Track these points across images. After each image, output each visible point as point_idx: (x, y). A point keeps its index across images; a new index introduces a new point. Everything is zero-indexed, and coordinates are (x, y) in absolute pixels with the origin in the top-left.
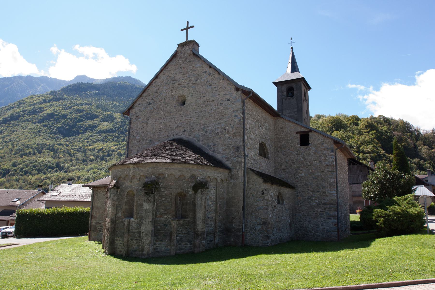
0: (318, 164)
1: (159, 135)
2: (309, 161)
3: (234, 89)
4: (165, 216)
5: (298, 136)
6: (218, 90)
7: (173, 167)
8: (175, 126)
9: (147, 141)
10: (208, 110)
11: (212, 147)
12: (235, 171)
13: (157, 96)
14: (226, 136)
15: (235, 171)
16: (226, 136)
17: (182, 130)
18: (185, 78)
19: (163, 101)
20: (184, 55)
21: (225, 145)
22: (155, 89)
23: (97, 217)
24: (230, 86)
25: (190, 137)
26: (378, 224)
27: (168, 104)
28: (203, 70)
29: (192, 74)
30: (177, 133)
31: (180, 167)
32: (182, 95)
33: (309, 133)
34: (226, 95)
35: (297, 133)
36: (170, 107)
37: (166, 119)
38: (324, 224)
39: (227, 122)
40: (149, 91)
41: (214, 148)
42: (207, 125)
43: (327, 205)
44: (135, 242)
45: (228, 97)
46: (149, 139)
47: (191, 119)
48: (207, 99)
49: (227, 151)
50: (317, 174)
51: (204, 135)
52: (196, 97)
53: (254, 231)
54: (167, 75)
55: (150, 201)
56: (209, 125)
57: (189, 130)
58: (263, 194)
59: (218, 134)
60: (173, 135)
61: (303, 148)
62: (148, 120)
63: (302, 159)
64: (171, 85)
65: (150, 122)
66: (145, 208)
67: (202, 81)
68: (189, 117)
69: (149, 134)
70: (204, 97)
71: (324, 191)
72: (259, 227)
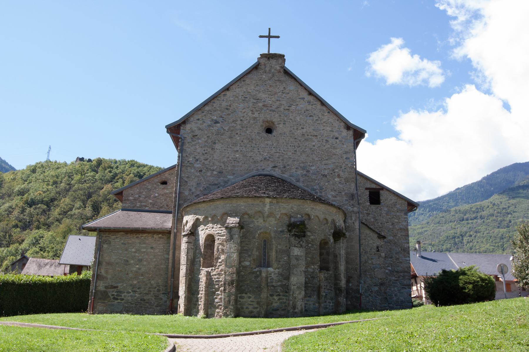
1: (233, 166)
3: (343, 127)
5: (367, 193)
6: (322, 124)
7: (317, 207)
8: (259, 158)
9: (215, 173)
10: (310, 146)
11: (317, 191)
12: (350, 221)
13: (229, 114)
14: (336, 180)
15: (350, 221)
16: (336, 180)
17: (272, 165)
18: (273, 99)
19: (239, 122)
20: (270, 71)
21: (335, 191)
22: (224, 104)
23: (109, 276)
24: (338, 122)
26: (467, 291)
27: (247, 127)
28: (299, 95)
29: (283, 96)
30: (263, 167)
31: (323, 208)
32: (269, 119)
34: (333, 132)
35: (367, 189)
36: (251, 132)
37: (246, 147)
38: (398, 294)
39: (337, 164)
40: (215, 105)
41: (321, 192)
42: (309, 164)
44: (276, 298)
45: (336, 135)
46: (218, 170)
47: (284, 152)
48: (306, 132)
49: (338, 198)
50: (389, 238)
51: (306, 175)
52: (291, 127)
53: (369, 293)
54: (245, 90)
55: (301, 246)
56: (311, 164)
57: (282, 166)
58: (378, 251)
60: (258, 170)
61: (373, 207)
62: (215, 143)
63: (372, 220)
64: (251, 105)
65: (218, 146)
66: (296, 254)
67: (299, 108)
68: (282, 149)
69: (217, 163)
70: (303, 128)
72: (376, 288)
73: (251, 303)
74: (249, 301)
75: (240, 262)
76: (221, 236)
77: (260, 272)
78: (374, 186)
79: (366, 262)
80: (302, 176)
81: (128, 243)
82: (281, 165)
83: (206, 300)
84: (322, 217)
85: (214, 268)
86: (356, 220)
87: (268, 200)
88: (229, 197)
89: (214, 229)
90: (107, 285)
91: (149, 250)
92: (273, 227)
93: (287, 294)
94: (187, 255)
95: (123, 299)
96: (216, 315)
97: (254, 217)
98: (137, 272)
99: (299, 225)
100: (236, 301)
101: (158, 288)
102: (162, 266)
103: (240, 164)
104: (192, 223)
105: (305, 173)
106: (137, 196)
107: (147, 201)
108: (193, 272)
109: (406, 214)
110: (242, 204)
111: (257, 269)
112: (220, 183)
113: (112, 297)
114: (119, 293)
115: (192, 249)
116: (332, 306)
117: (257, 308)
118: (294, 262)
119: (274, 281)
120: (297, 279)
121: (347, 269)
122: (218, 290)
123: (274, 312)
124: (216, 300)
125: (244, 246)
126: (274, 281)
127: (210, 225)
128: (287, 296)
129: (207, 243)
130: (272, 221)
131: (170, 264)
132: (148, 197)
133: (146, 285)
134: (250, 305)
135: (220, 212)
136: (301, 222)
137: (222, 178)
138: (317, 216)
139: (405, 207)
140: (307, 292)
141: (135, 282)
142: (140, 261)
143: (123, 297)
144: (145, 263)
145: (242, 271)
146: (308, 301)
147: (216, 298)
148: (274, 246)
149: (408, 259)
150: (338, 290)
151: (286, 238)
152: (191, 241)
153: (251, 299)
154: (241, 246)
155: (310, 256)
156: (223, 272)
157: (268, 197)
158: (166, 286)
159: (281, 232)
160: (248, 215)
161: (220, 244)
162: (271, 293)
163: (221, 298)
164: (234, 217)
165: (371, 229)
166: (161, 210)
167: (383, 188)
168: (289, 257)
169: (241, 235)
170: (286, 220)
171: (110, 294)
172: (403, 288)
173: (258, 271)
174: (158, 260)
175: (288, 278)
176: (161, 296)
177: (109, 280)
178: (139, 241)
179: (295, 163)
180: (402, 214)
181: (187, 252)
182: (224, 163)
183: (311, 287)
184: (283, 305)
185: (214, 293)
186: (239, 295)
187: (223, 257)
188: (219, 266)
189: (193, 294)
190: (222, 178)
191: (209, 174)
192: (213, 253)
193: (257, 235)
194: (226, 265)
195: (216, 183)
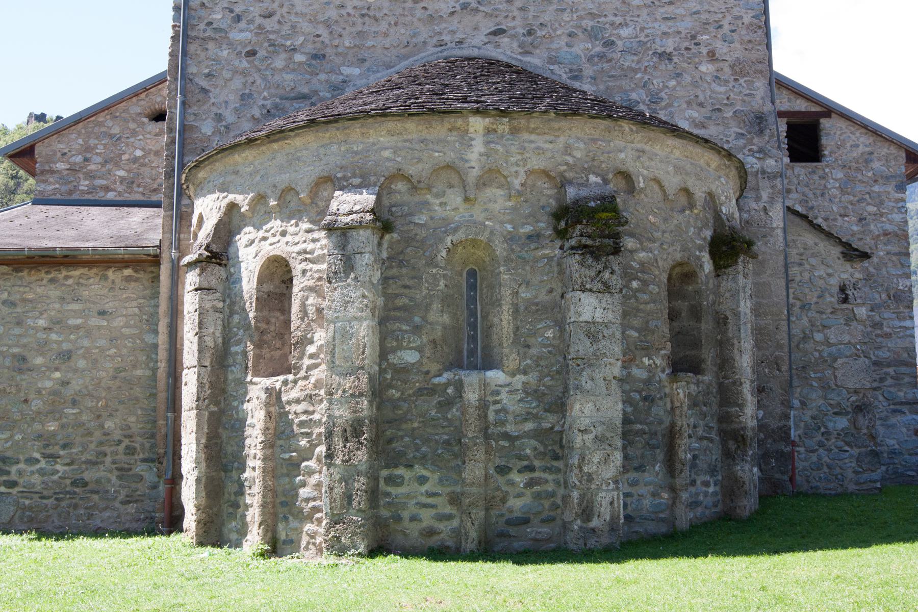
0: (855, 228)
1: (359, 33)
2: (823, 214)
4: (646, 361)
7: (657, 148)
9: (299, 58)
12: (754, 205)
14: (703, 68)
15: (754, 205)
16: (703, 68)
21: (701, 105)
25: (527, 59)
30: (459, 36)
33: (823, 121)
39: (703, 17)
42: (611, 18)
43: (889, 366)
44: (520, 479)
46: (309, 48)
51: (601, 56)
53: (819, 437)
55: (607, 288)
56: (618, 20)
58: (845, 300)
59: (665, 56)
61: (801, 170)
66: (586, 316)
69: (305, 26)
71: (877, 318)
72: (842, 423)
73: (430, 500)
74: (420, 493)
75: (383, 354)
76: (313, 262)
77: (459, 386)
78: (801, 106)
79: (805, 338)
80: (590, 59)
81: (24, 300)
82: (518, 25)
83: (268, 491)
84: (673, 183)
85: (291, 377)
86: (772, 200)
87: (477, 124)
88: (336, 119)
89: (288, 238)
91: (95, 321)
92: (502, 223)
93: (559, 464)
94: (200, 335)
95: (14, 484)
96: (303, 544)
97: (429, 188)
98: (55, 393)
99: (594, 211)
100: (373, 494)
101: (126, 442)
102: (139, 372)
103: (383, 27)
104: (214, 221)
105: (598, 49)
106: (79, 159)
107: (109, 172)
108: (224, 391)
109: (901, 188)
110: (385, 142)
111: (446, 376)
112: (316, 92)
115: (216, 310)
116: (715, 493)
117: (449, 517)
118: (581, 346)
119: (510, 418)
120: (594, 409)
121: (758, 364)
122: (307, 454)
123: (512, 531)
124: (304, 492)
125: (397, 296)
126: (510, 418)
127: (276, 224)
128: (558, 470)
129: (267, 287)
130: (497, 200)
131: (162, 366)
133: (89, 433)
134: (425, 506)
135: (304, 176)
136: (602, 198)
137: (323, 77)
138: (657, 181)
139: (900, 167)
140: (631, 451)
141: (52, 427)
142: (66, 356)
143: (14, 477)
144: (82, 364)
145: (390, 386)
146: (634, 483)
147: (304, 484)
148: (506, 292)
149: (907, 323)
150: (731, 438)
151: (550, 259)
152: (214, 283)
153: (424, 489)
154: (385, 295)
155: (636, 322)
156: (322, 392)
157: (477, 112)
158: (153, 436)
159: (530, 237)
160: (407, 179)
161: (311, 289)
162: (498, 462)
163: (318, 485)
164: (358, 188)
165: (818, 228)
167: (829, 110)
168: (562, 330)
169: (385, 255)
170: (547, 194)
172: (895, 411)
173: (448, 384)
174: (125, 351)
175: (560, 406)
176: (140, 468)
178: (58, 293)
179: (566, 17)
180: (890, 189)
181: (200, 323)
182: (327, 24)
183: (645, 437)
184: (547, 504)
185: (294, 466)
186: (384, 473)
187: (321, 336)
188: (310, 368)
189: (226, 469)
190: (323, 77)
191: (279, 62)
192: (288, 322)
193: (444, 253)
194: (332, 367)
195: (305, 90)
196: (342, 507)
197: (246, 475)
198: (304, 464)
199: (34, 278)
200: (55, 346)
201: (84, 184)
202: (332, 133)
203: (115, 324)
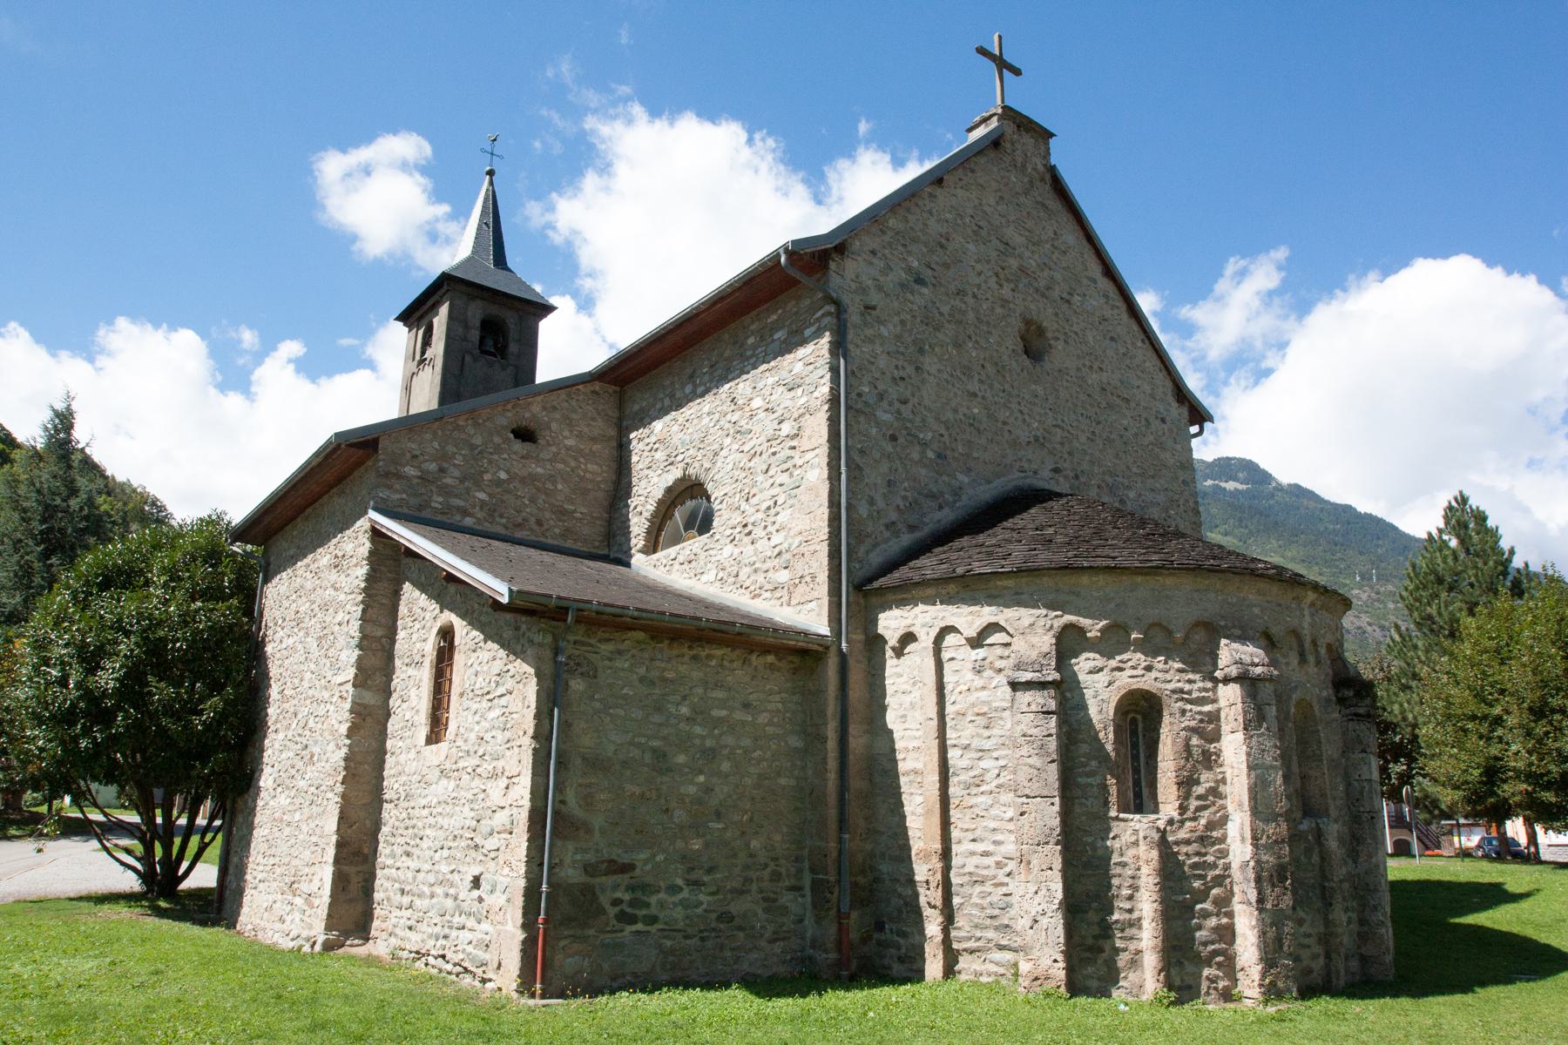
23: (598, 822)
62: (921, 351)
81: (665, 680)
89: (1154, 674)
90: (590, 857)
91: (739, 715)
95: (653, 920)
96: (1204, 986)
102: (783, 781)
103: (983, 441)
106: (433, 467)
107: (468, 491)
113: (612, 911)
114: (639, 894)
132: (473, 478)
133: (735, 856)
141: (696, 845)
142: (711, 754)
143: (654, 911)
147: (1200, 927)
161: (1193, 730)
166: (519, 534)
171: (604, 900)
176: (786, 899)
177: (597, 834)
185: (1188, 909)
188: (1198, 809)
196: (1275, 951)
197: (1116, 917)
198: (1198, 907)
199: (675, 652)
200: (697, 742)
201: (437, 501)
202: (1216, 582)
203: (760, 720)
